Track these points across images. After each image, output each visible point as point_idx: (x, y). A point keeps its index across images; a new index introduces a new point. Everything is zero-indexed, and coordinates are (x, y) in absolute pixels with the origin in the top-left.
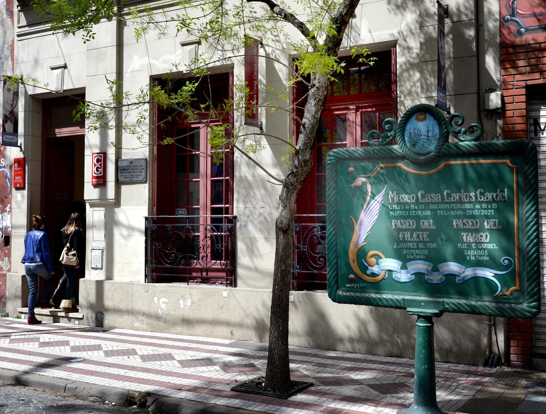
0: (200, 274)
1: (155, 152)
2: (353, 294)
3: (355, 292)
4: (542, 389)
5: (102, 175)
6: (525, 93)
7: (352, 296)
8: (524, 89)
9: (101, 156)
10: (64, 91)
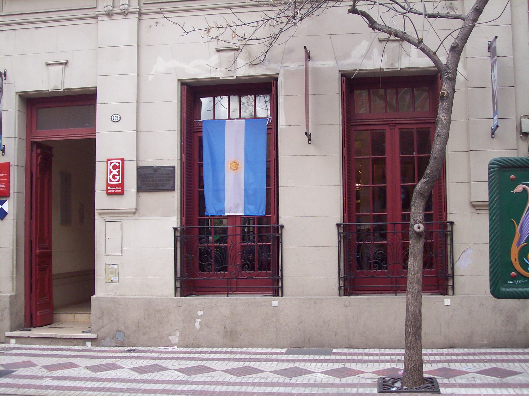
0: (449, 287)
1: (184, 160)
2: (516, 290)
3: (517, 287)
4: (526, 350)
5: (120, 182)
6: (211, 99)
7: (516, 292)
8: (231, 96)
9: (119, 163)
10: (64, 89)
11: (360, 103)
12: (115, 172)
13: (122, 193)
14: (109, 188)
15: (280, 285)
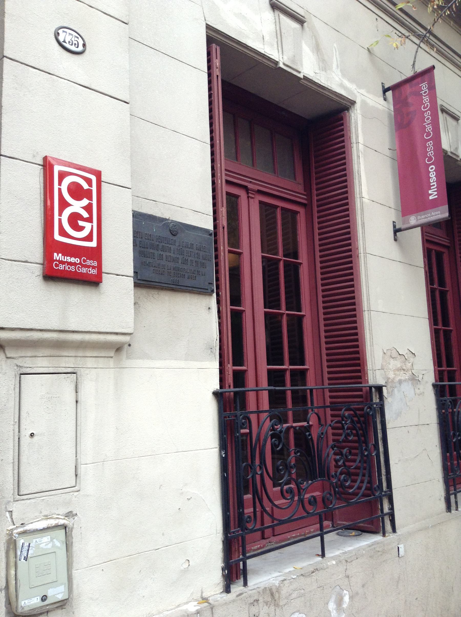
9: (89, 181)
11: (137, 7)
12: (77, 206)
13: (94, 282)
14: (57, 256)
15: (386, 509)
